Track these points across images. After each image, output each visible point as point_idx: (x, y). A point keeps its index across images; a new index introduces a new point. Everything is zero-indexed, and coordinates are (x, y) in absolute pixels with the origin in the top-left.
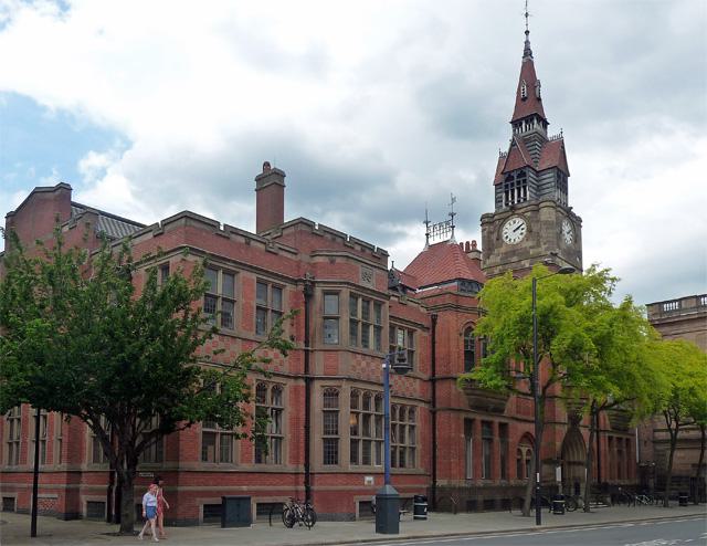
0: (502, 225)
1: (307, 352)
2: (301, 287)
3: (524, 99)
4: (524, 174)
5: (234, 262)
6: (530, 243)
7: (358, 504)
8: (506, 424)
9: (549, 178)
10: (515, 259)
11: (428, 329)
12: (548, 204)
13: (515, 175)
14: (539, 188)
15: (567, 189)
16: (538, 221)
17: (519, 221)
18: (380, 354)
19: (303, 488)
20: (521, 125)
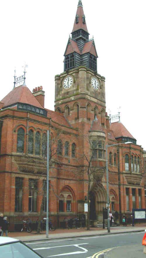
0: (63, 80)
6: (75, 88)
12: (84, 69)
13: (69, 56)
17: (70, 78)
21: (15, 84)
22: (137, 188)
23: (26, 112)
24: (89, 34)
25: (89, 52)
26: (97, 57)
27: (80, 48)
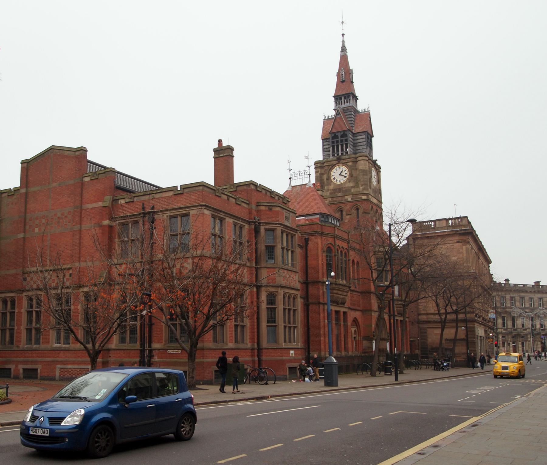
0: (331, 169)
1: (257, 269)
2: (253, 227)
3: (343, 82)
4: (346, 135)
5: (224, 213)
6: (351, 184)
7: (288, 369)
8: (522, 327)
9: (362, 139)
10: (340, 194)
11: (303, 247)
12: (364, 158)
13: (339, 135)
14: (355, 145)
15: (371, 145)
16: (356, 169)
18: (294, 269)
19: (256, 359)
20: (341, 99)
21: (290, 180)
22: (342, 310)
23: (333, 227)
24: (377, 160)
25: (367, 131)
26: (373, 137)
27: (350, 122)
